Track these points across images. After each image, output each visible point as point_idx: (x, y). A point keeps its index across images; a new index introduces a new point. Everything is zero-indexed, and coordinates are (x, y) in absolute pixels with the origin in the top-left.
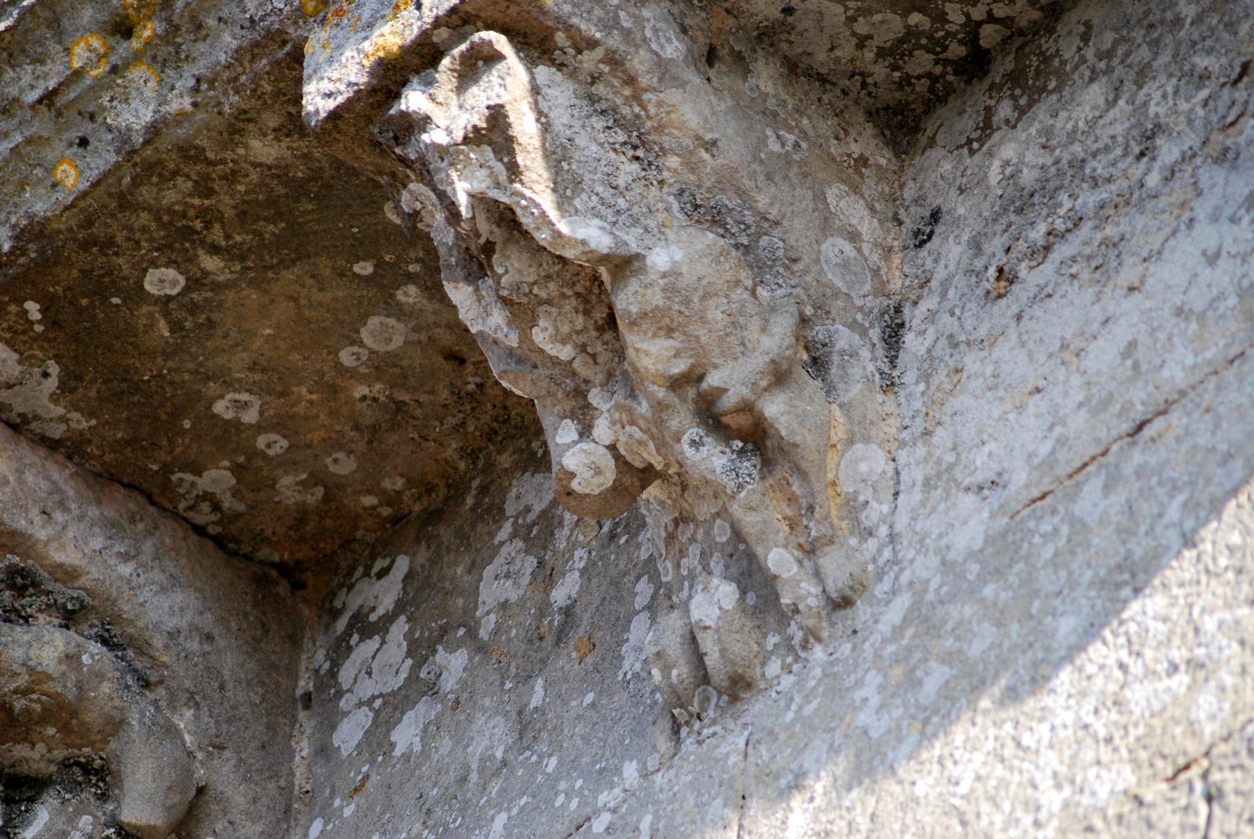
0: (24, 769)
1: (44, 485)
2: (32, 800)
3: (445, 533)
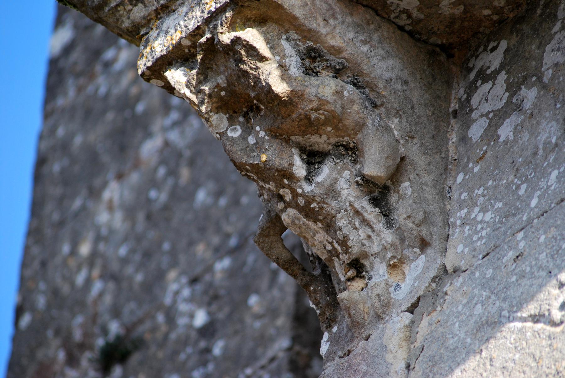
0: (316, 148)
1: (325, 6)
2: (320, 163)
3: (526, 28)
